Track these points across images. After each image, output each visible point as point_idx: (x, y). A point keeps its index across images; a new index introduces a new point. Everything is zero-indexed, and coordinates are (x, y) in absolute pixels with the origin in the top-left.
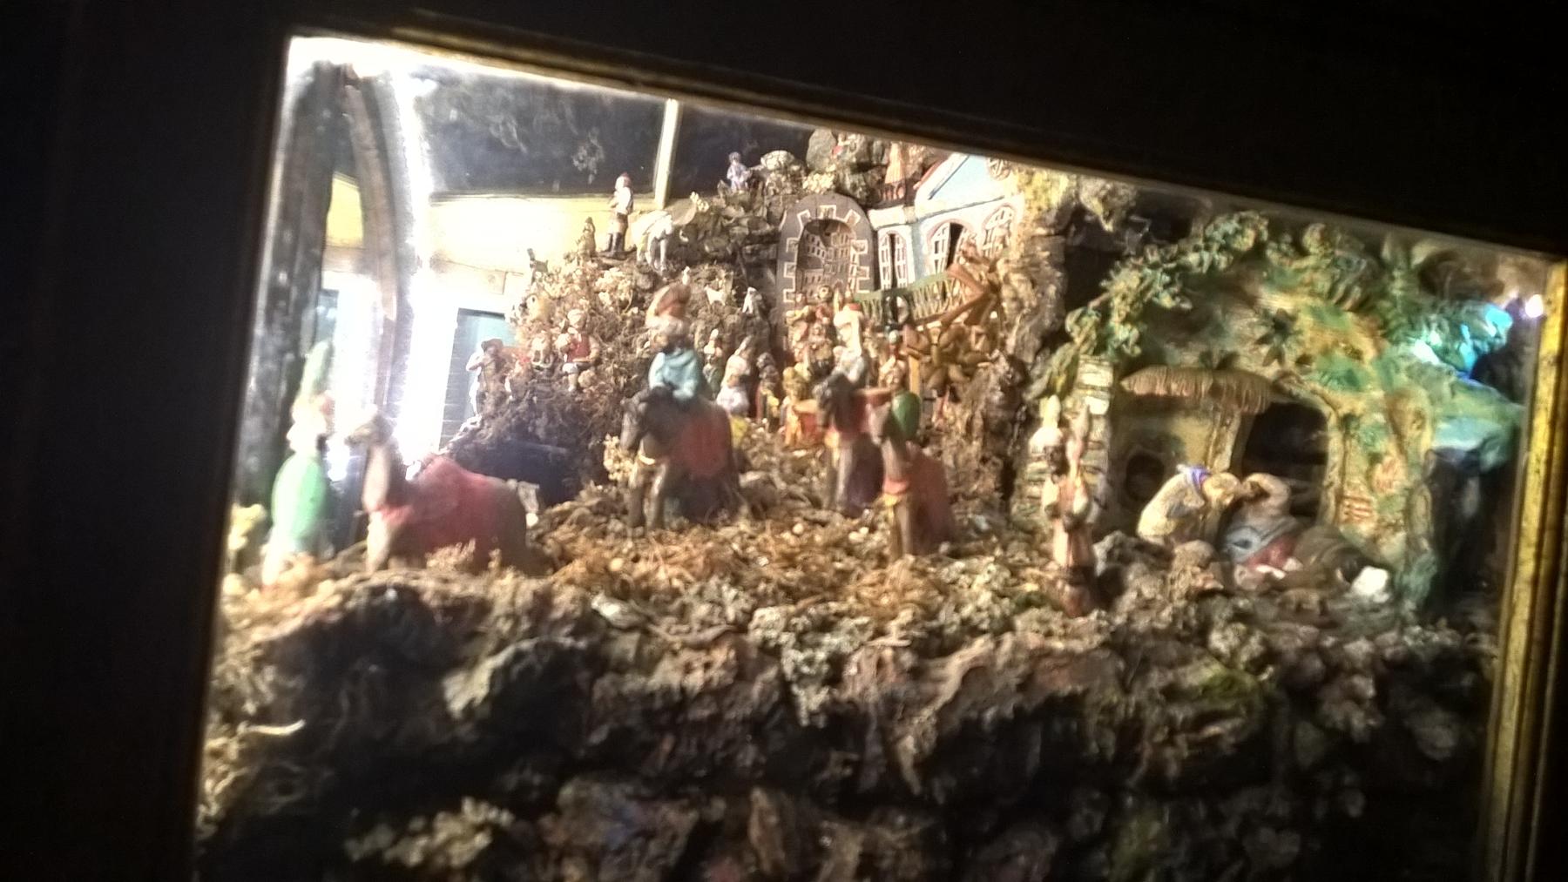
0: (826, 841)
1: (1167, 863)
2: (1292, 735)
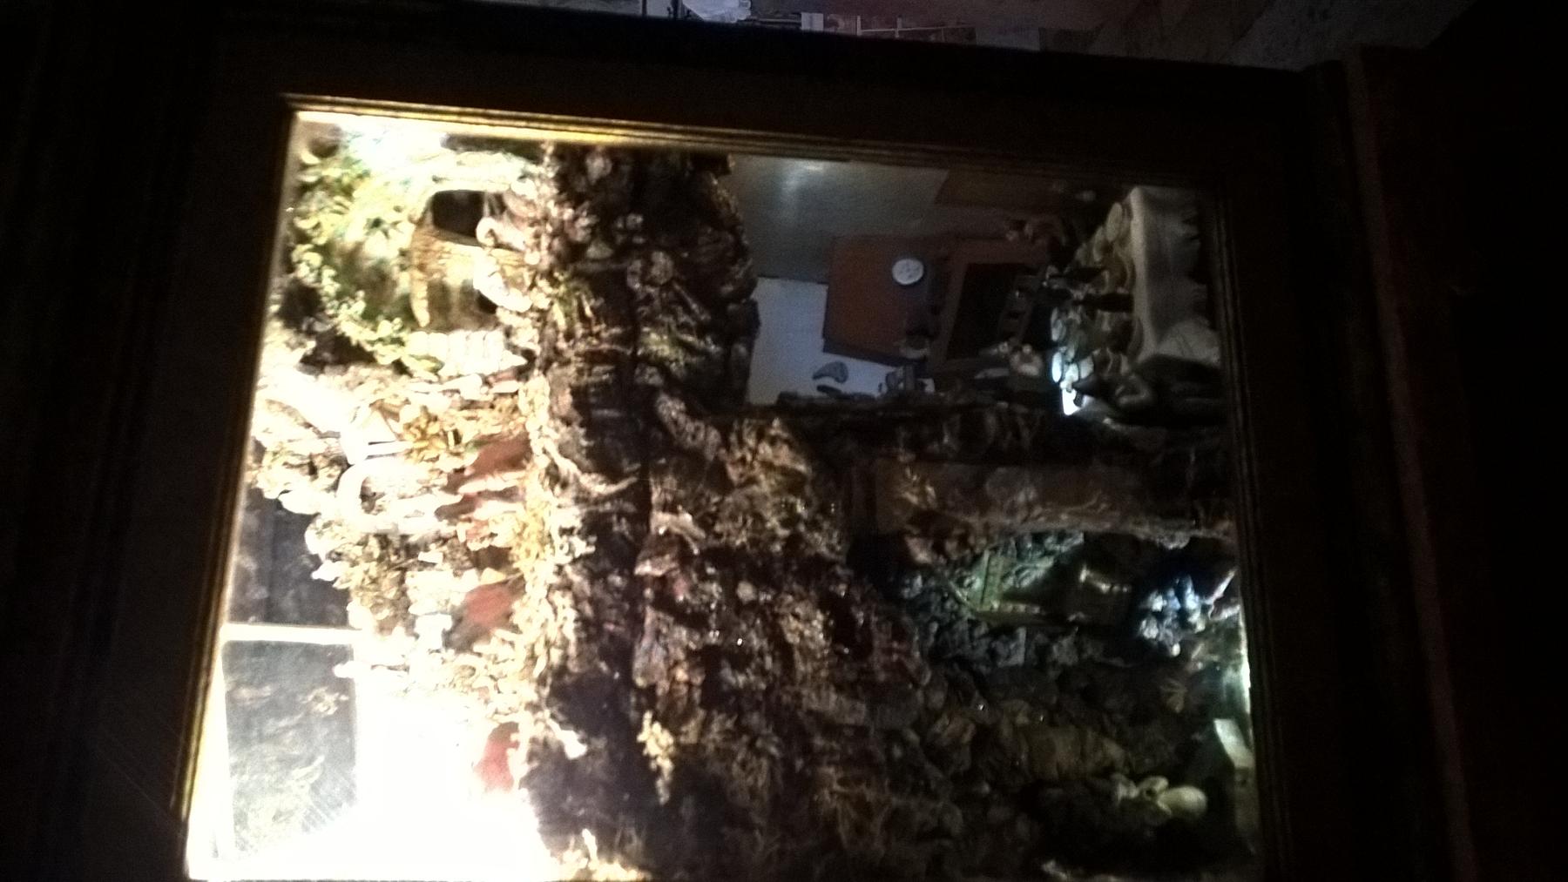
0: (662, 531)
1: (673, 328)
2: (594, 261)
